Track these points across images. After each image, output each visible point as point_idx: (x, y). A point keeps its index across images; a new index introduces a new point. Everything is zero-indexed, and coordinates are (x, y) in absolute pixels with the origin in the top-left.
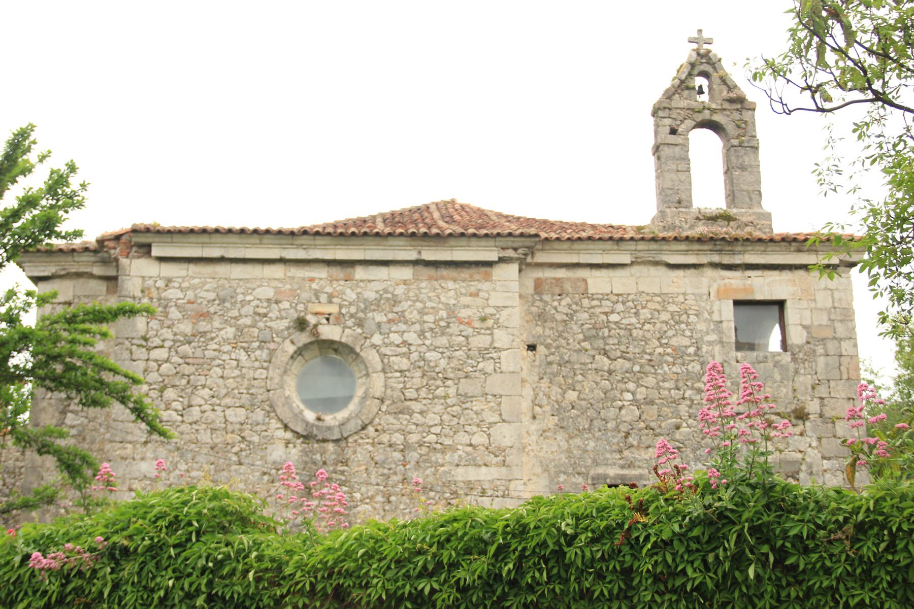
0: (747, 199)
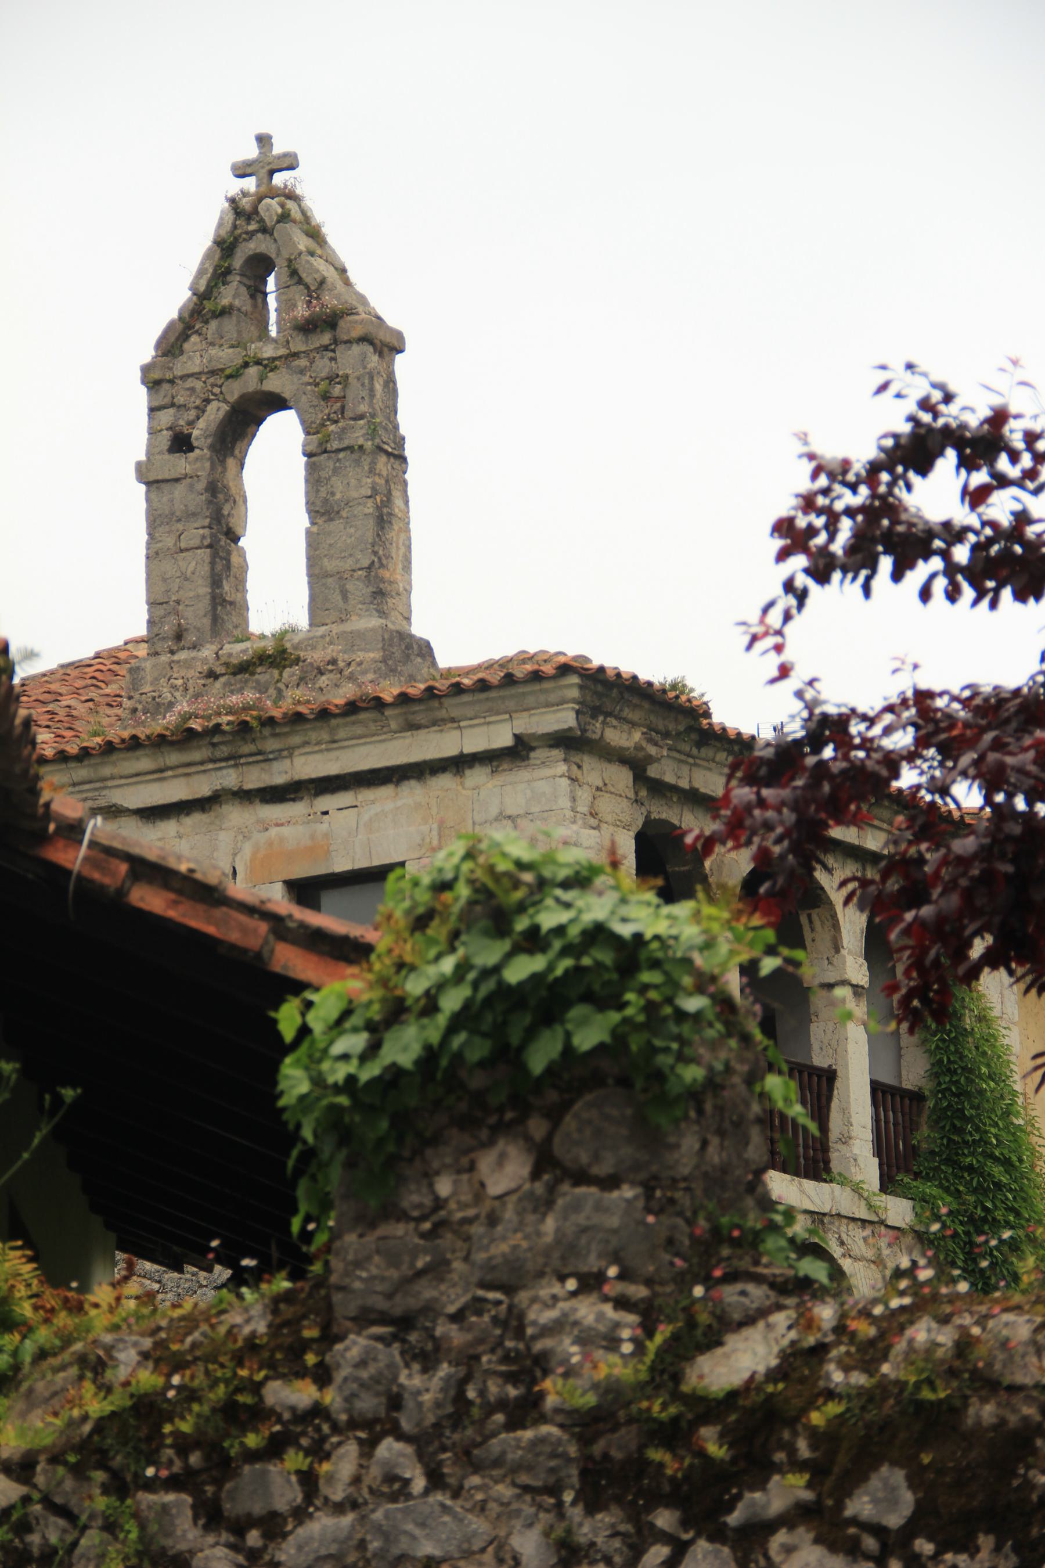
0: (337, 597)
